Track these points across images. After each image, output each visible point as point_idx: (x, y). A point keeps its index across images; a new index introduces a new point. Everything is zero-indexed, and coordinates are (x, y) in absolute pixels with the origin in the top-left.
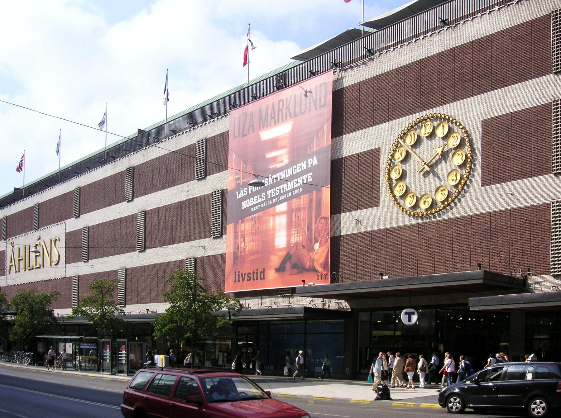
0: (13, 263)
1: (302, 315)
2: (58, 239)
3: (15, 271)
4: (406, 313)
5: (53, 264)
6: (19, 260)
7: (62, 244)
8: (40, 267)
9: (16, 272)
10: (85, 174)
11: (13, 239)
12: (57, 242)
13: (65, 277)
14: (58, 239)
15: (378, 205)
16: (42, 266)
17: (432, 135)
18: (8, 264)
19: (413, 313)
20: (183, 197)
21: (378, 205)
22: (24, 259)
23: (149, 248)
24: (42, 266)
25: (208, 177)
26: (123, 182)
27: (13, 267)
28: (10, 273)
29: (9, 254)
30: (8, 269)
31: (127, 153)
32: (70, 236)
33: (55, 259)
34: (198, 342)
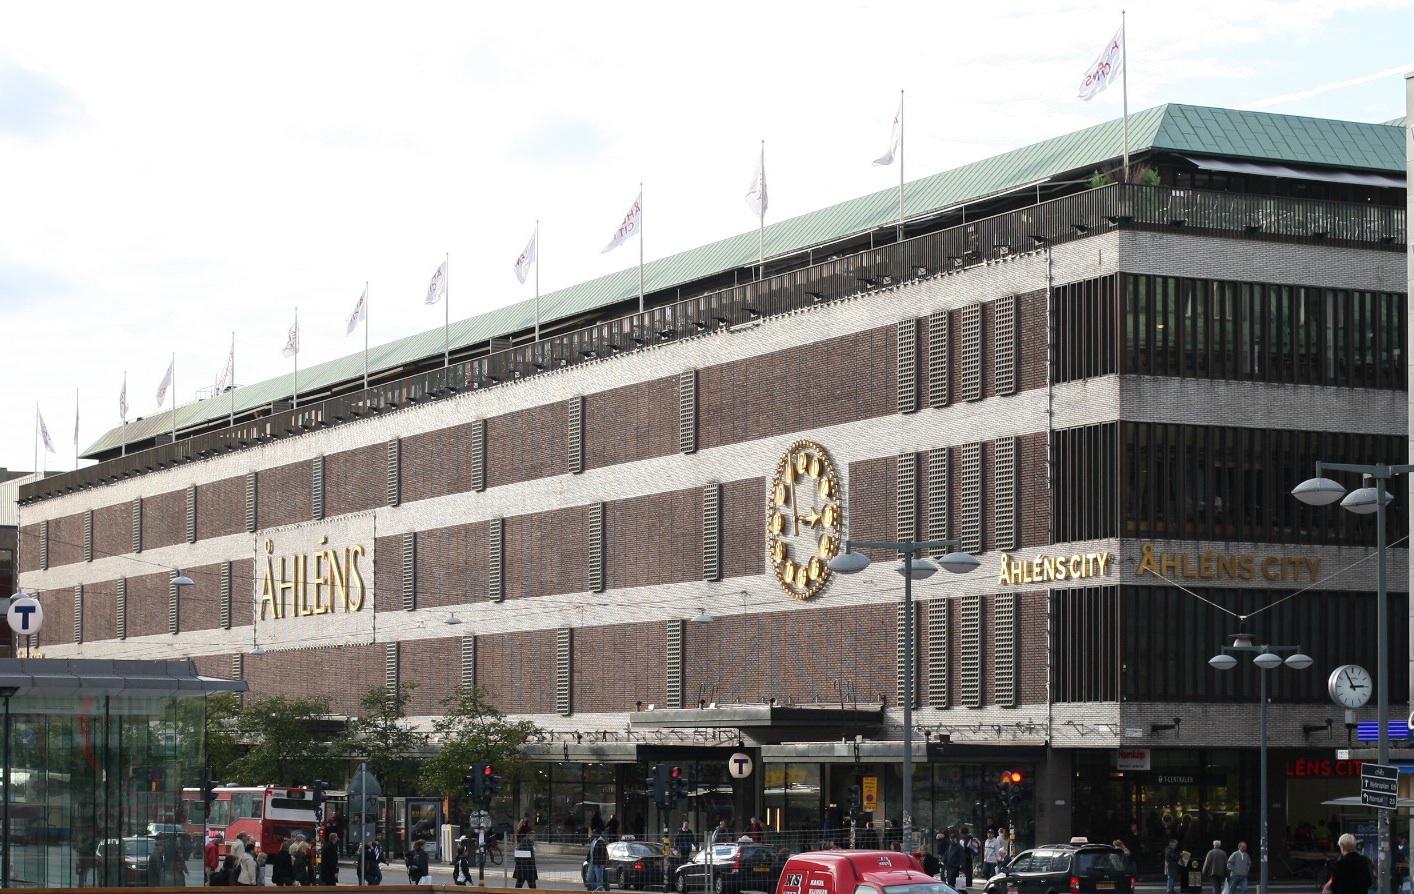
0: (270, 596)
1: (635, 758)
2: (359, 550)
3: (274, 616)
4: (736, 761)
5: (353, 608)
6: (283, 589)
7: (367, 564)
8: (326, 612)
9: (277, 618)
10: (898, 288)
11: (268, 533)
12: (360, 556)
13: (374, 643)
14: (359, 550)
15: (764, 573)
16: (329, 611)
17: (797, 477)
18: (260, 596)
19: (746, 761)
20: (554, 504)
21: (764, 573)
22: (293, 589)
23: (1028, 545)
24: (329, 611)
25: (700, 452)
26: (890, 359)
27: (270, 607)
28: (263, 619)
29: (261, 570)
30: (259, 608)
31: (1002, 253)
32: (385, 548)
33: (355, 596)
34: (329, 793)
